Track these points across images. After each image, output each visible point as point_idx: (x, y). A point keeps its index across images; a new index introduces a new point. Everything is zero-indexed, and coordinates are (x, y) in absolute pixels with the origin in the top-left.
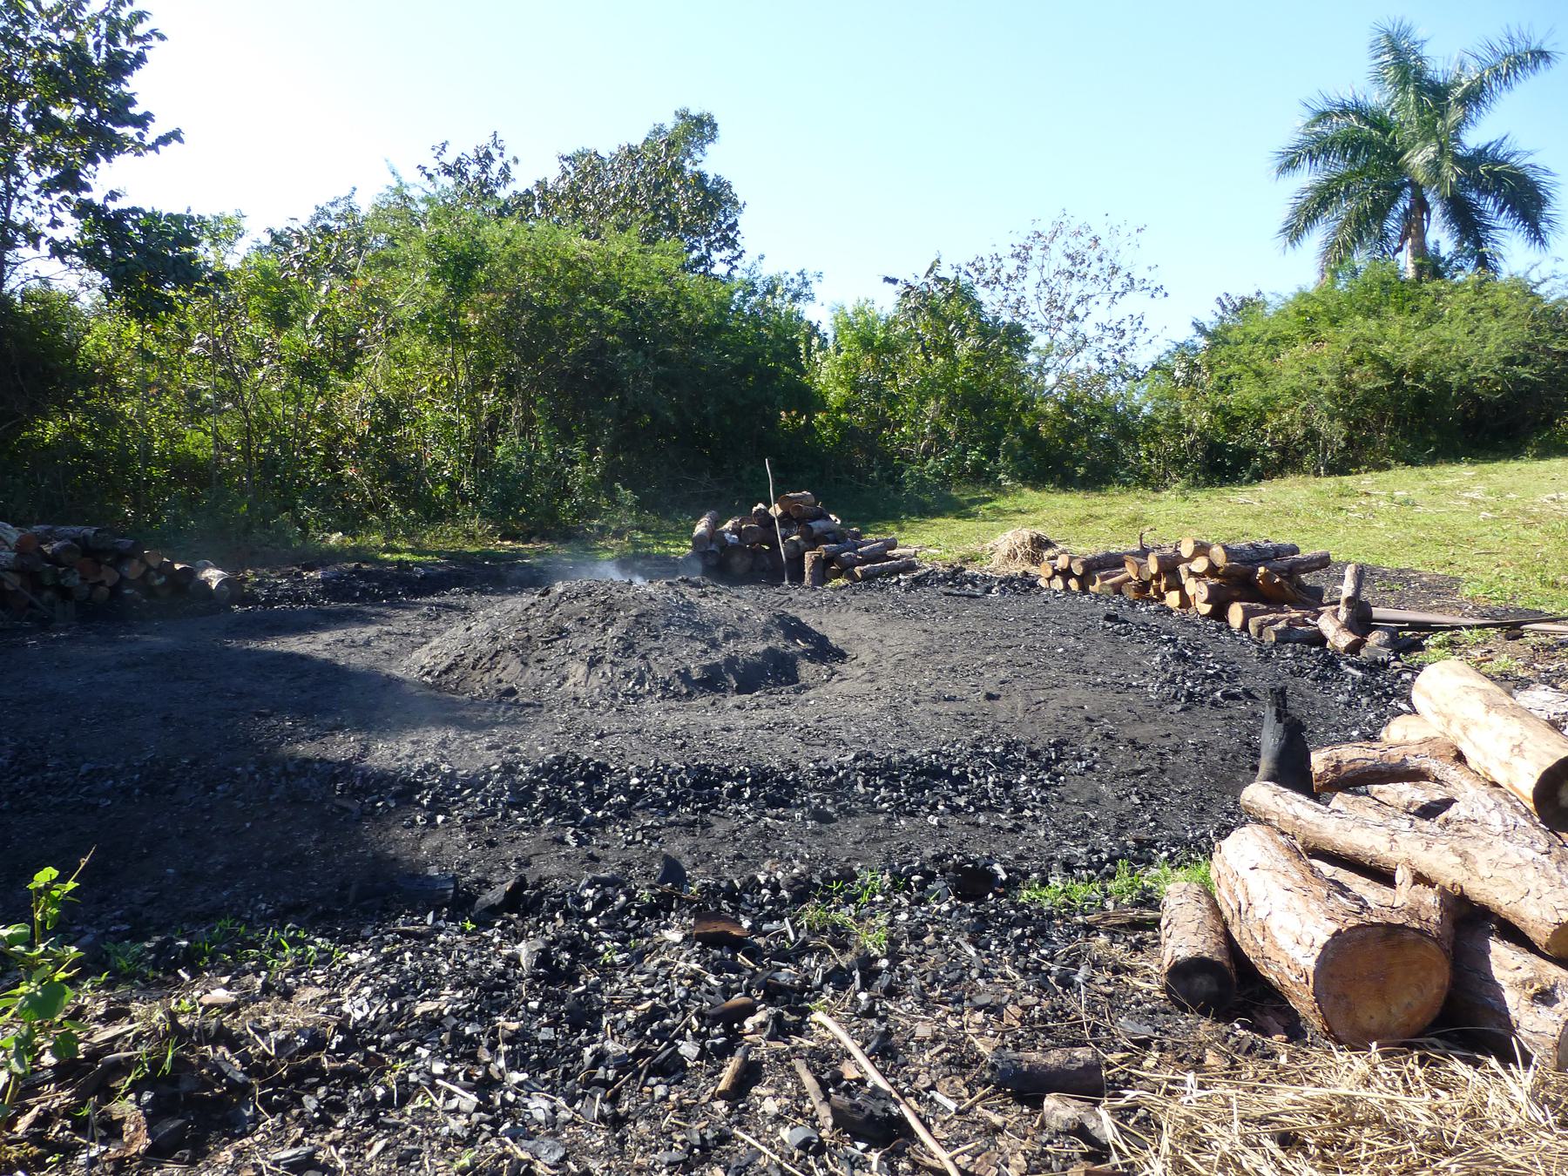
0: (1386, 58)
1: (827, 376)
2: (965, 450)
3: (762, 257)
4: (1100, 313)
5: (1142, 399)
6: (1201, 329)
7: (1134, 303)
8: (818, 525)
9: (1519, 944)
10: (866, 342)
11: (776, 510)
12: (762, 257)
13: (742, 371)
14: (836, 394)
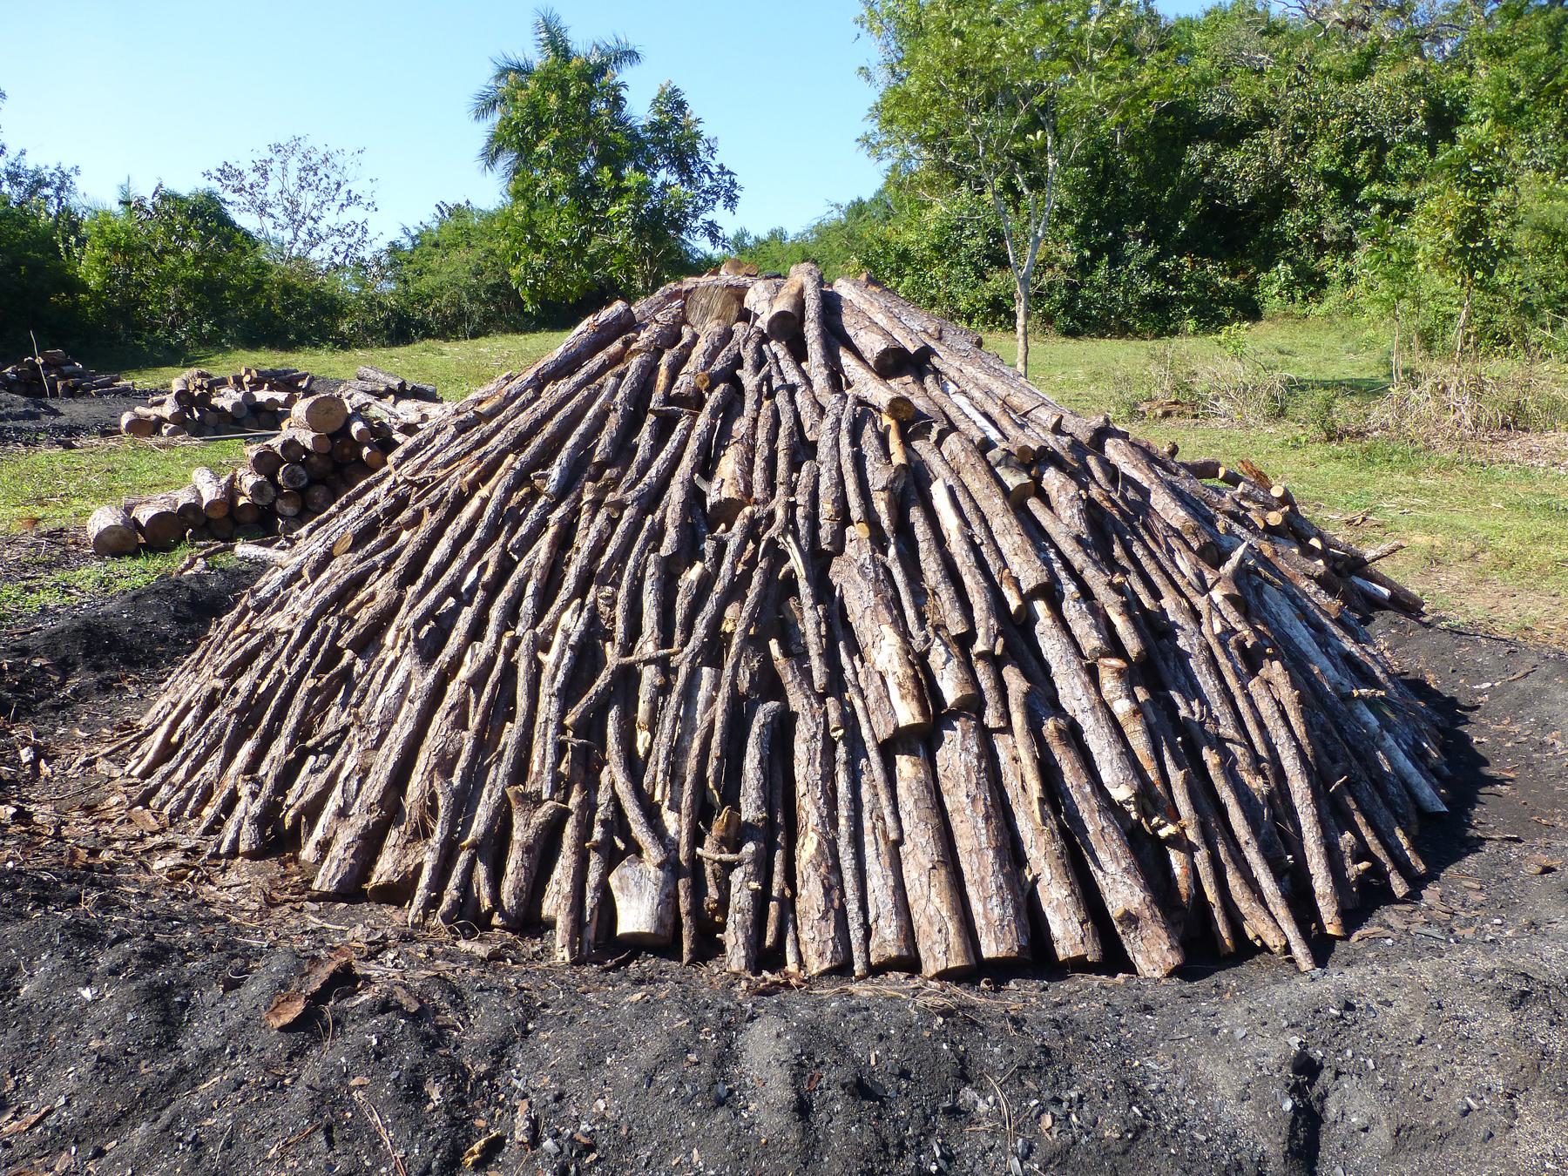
0: (543, 35)
1: (89, 268)
2: (200, 322)
3: (23, 153)
4: (331, 218)
5: (346, 286)
6: (406, 231)
7: (354, 213)
8: (67, 369)
9: (1253, 892)
10: (114, 247)
11: (40, 361)
12: (23, 153)
13: (14, 266)
14: (94, 282)
